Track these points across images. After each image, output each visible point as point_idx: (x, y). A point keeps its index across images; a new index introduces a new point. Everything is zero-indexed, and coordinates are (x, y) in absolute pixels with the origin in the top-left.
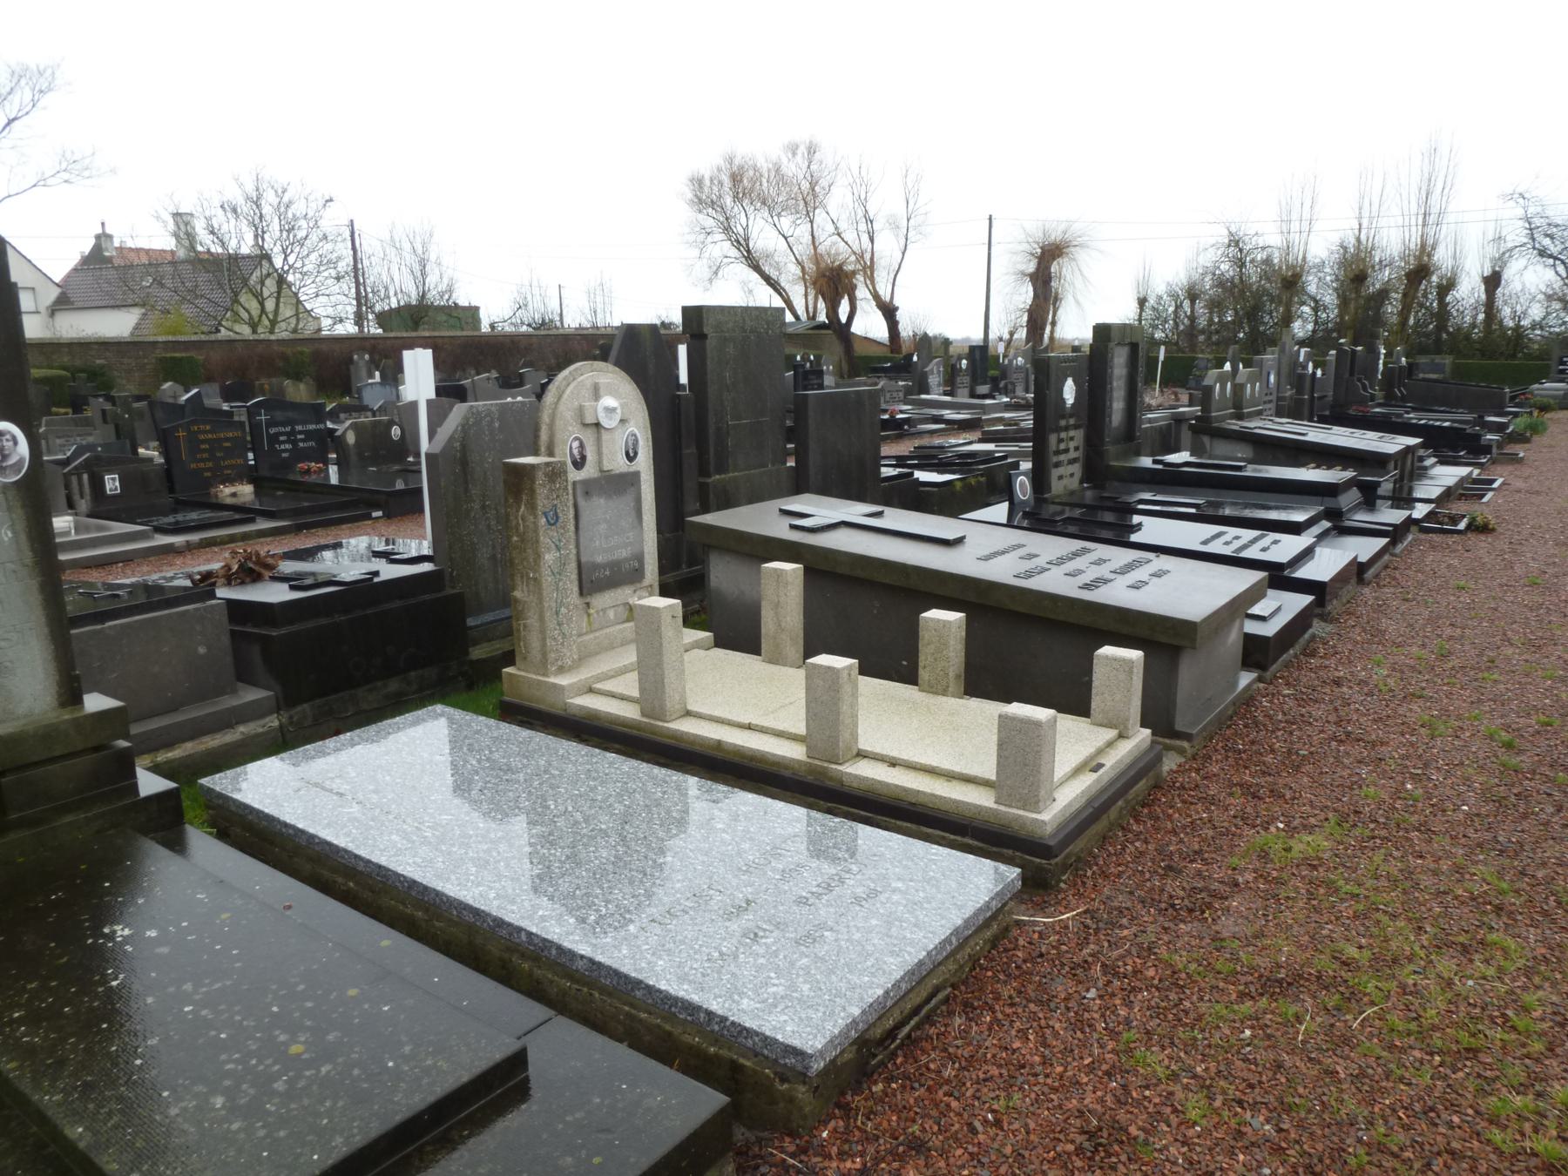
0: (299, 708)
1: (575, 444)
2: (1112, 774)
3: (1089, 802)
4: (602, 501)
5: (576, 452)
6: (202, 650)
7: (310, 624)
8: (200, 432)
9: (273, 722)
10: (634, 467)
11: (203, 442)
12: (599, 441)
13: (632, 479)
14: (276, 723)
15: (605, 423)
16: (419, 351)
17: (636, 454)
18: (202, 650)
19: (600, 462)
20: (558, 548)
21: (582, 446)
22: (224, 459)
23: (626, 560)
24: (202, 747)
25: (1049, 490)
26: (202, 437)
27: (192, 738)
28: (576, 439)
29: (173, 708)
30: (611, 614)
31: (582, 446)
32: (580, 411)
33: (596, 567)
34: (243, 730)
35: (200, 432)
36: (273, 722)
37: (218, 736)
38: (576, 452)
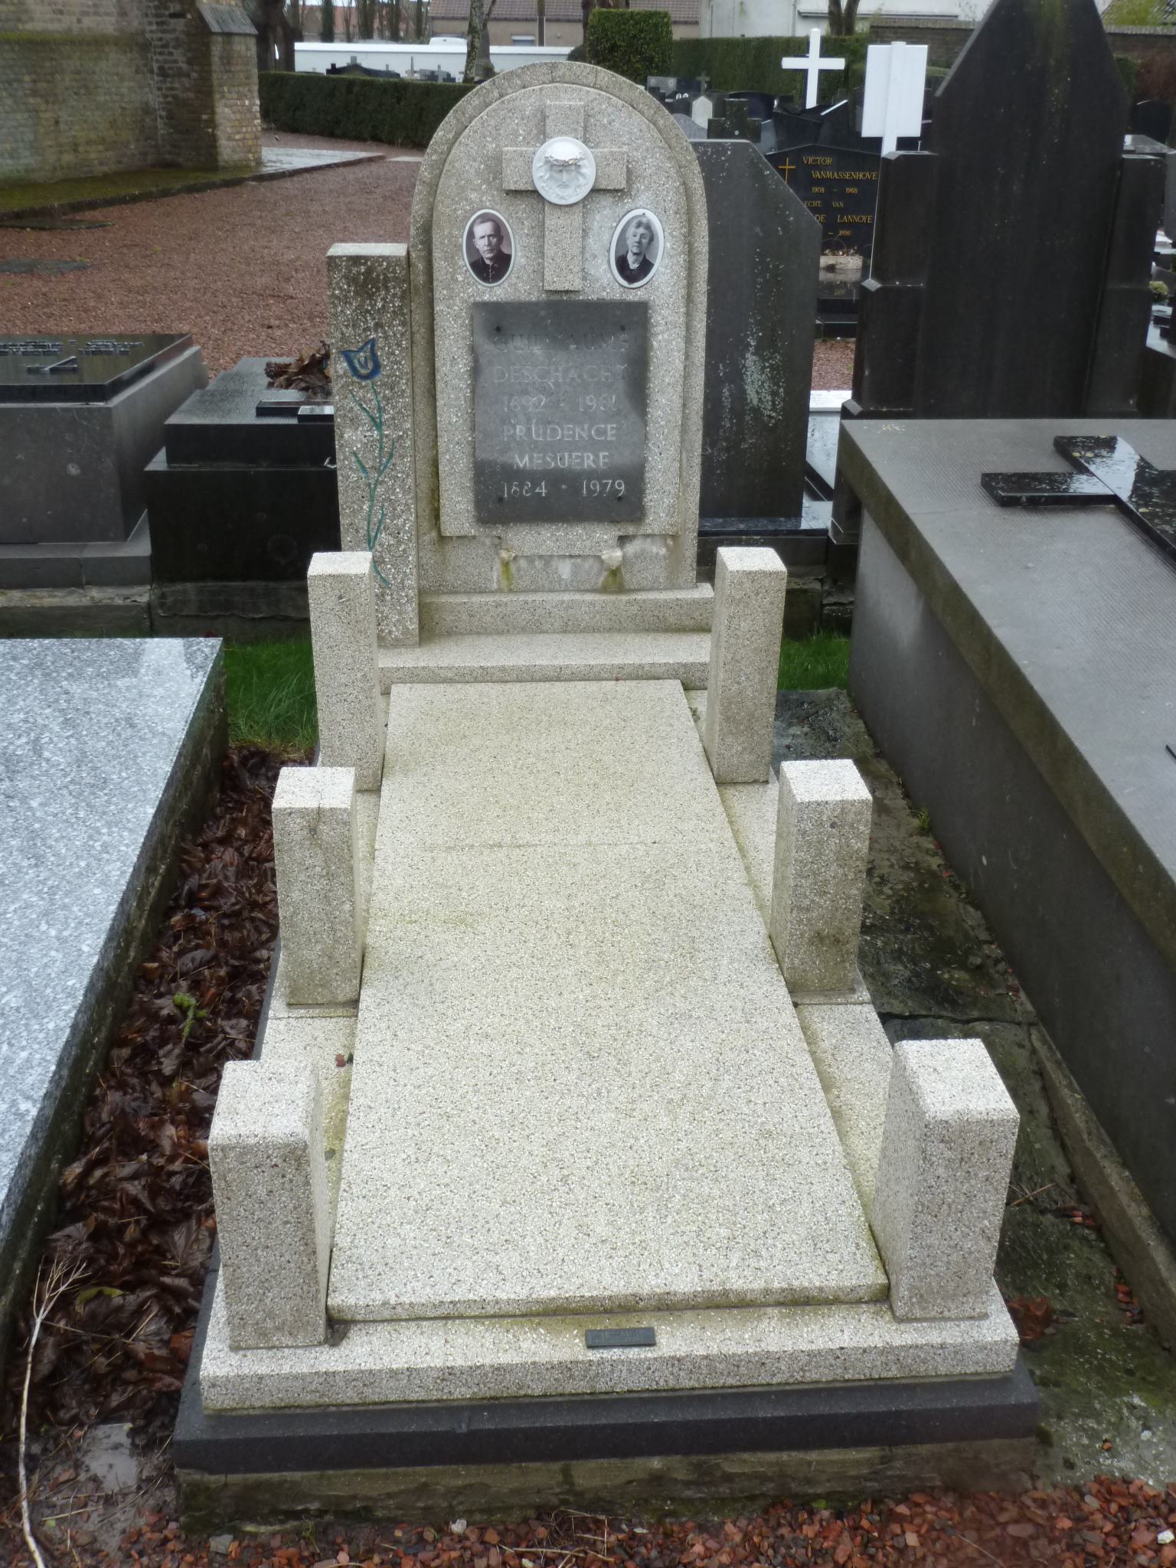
0: (179, 587)
1: (483, 230)
2: (664, 1380)
3: (494, 1405)
4: (537, 350)
5: (482, 244)
6: (73, 470)
7: (228, 467)
8: (816, 167)
9: (143, 595)
10: (636, 293)
11: (819, 182)
12: (540, 231)
13: (632, 320)
14: (144, 599)
15: (552, 193)
16: (899, 46)
17: (646, 266)
18: (73, 470)
19: (540, 272)
20: (378, 424)
21: (499, 233)
22: (843, 212)
23: (591, 474)
24: (36, 602)
25: (824, 532)
26: (817, 175)
27: (22, 586)
28: (485, 218)
29: (30, 539)
30: (565, 569)
31: (499, 233)
32: (495, 167)
33: (511, 473)
34: (96, 594)
35: (816, 167)
36: (143, 595)
37: (59, 593)
38: (482, 244)
